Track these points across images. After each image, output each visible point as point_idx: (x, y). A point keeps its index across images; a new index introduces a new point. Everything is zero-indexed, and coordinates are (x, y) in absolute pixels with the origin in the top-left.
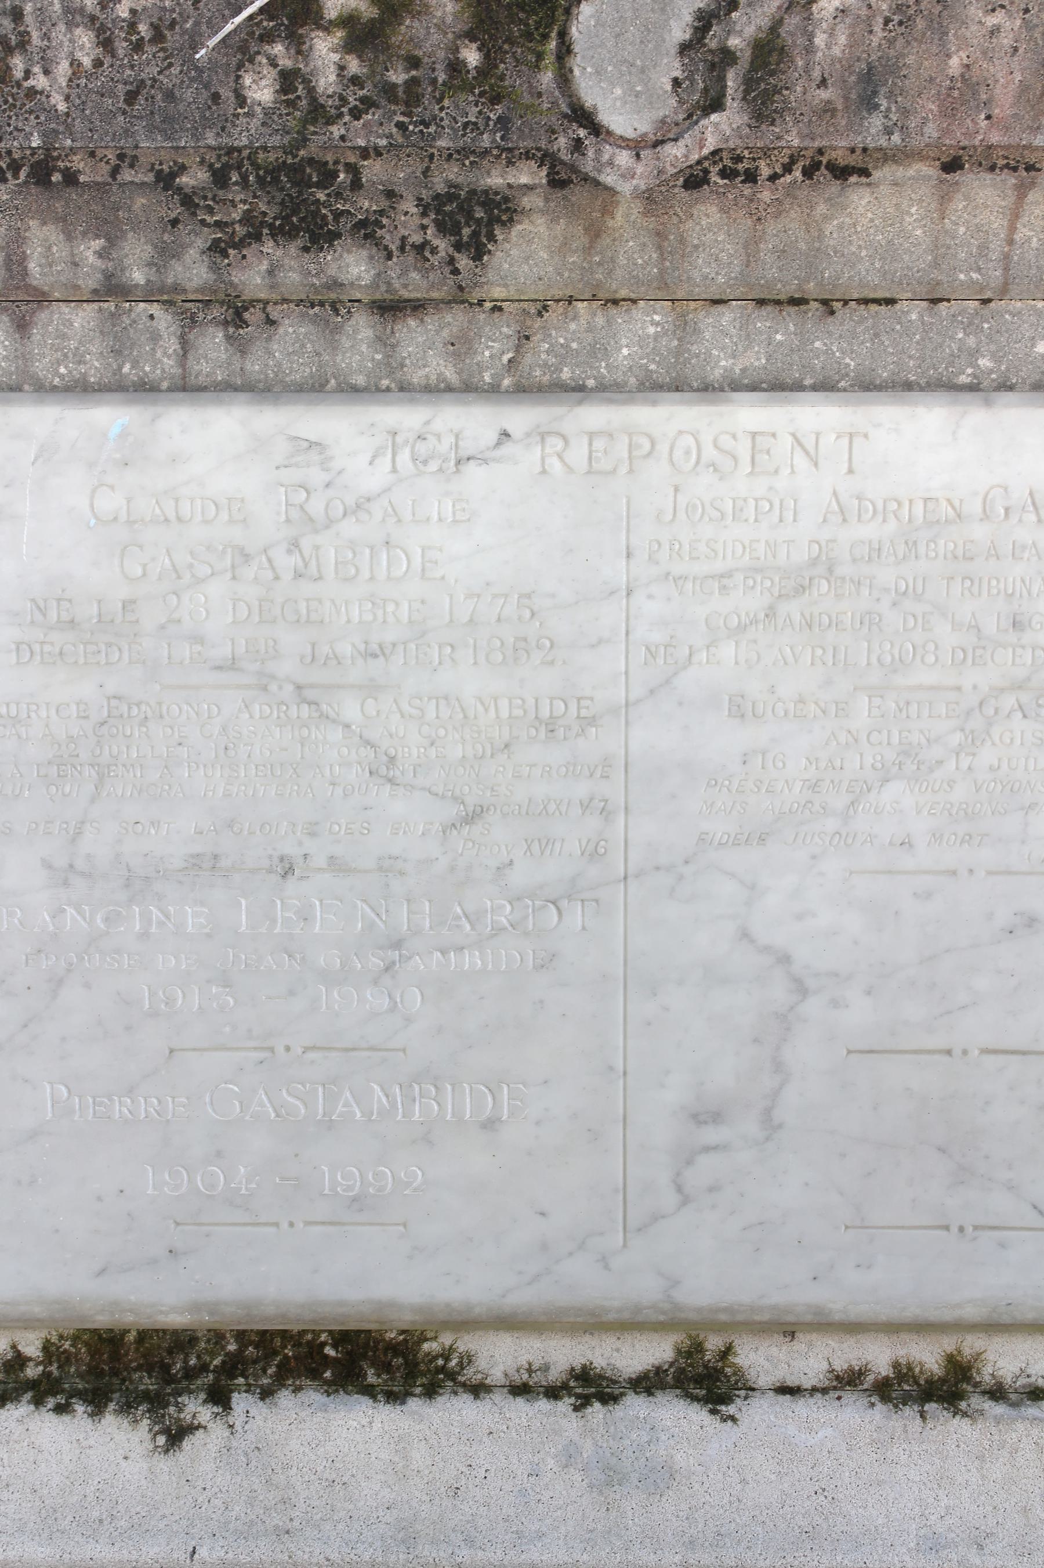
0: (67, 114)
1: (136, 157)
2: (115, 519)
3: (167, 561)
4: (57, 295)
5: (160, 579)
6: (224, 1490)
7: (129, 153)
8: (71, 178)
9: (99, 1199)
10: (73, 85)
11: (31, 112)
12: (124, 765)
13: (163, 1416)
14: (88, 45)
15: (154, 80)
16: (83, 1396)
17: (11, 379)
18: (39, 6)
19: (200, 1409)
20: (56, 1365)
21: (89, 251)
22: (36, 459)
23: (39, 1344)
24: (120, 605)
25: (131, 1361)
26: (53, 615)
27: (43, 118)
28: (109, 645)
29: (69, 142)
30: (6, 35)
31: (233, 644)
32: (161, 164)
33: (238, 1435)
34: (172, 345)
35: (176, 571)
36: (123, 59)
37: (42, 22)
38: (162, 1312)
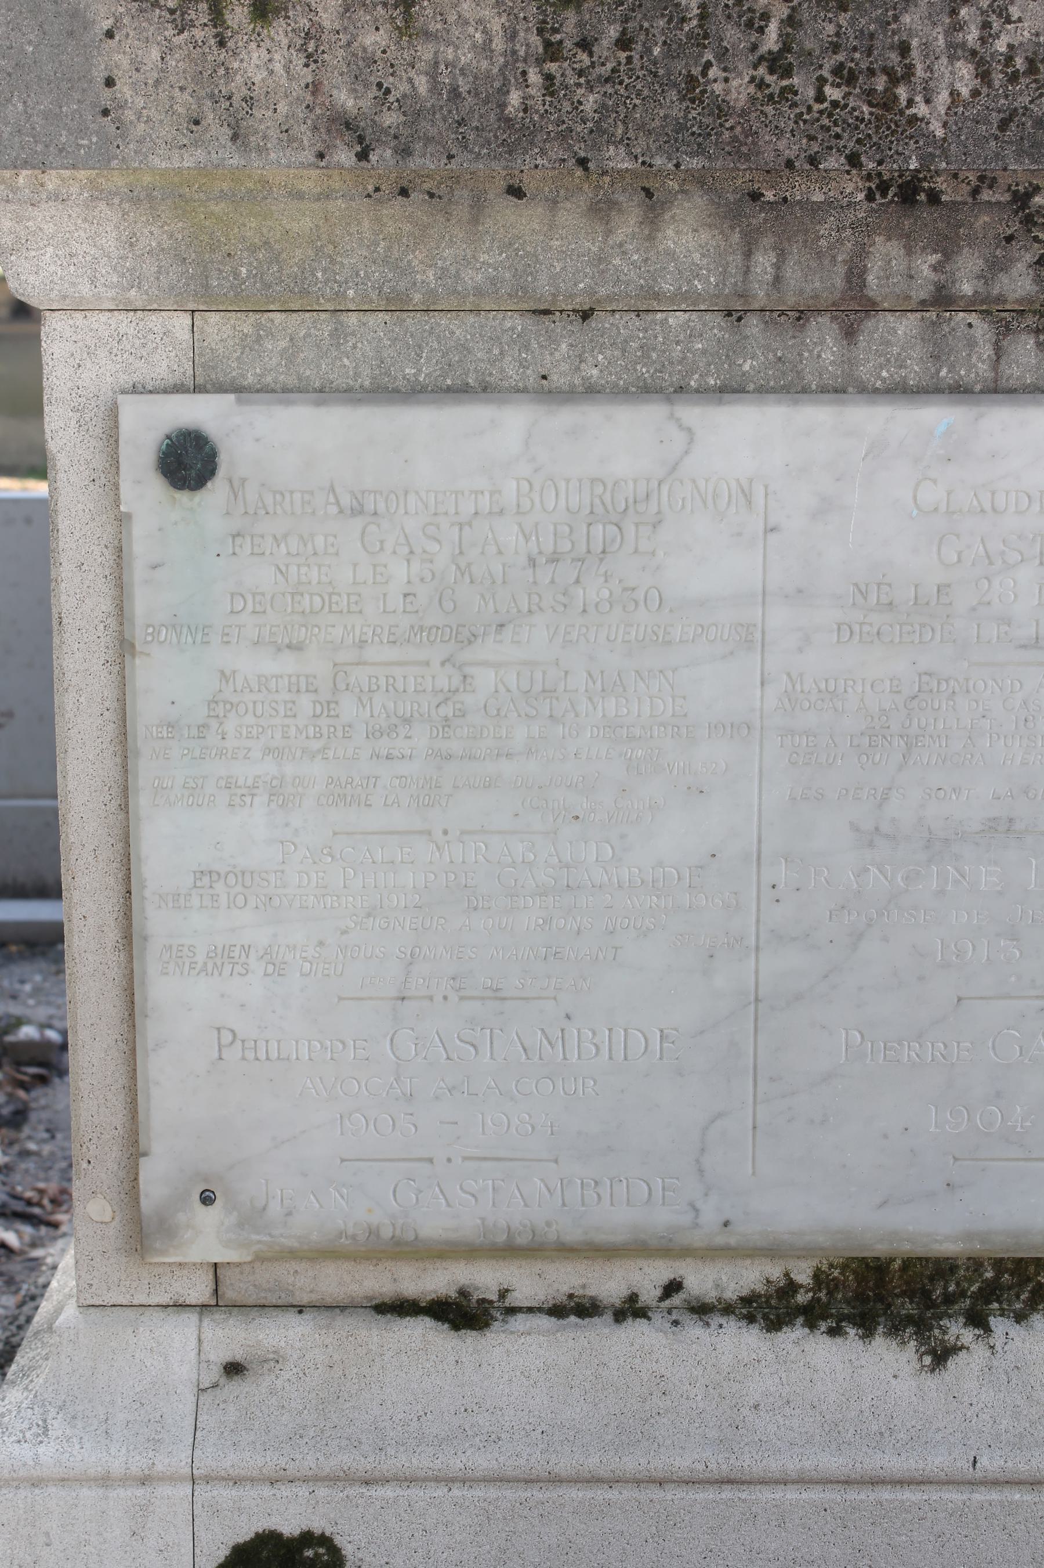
0: (944, 140)
1: (995, 178)
2: (936, 509)
3: (981, 548)
4: (886, 305)
5: (973, 564)
6: (989, 1405)
7: (988, 174)
8: (934, 198)
9: (885, 1136)
10: (952, 113)
11: (911, 137)
12: (931, 736)
13: (929, 1338)
14: (967, 77)
15: (1026, 108)
16: (851, 1319)
17: (837, 381)
18: (924, 41)
19: (962, 1331)
20: (824, 1292)
21: (925, 264)
22: (866, 455)
23: (810, 1272)
24: (935, 589)
25: (895, 1288)
26: (873, 599)
27: (921, 143)
28: (923, 625)
29: (944, 165)
30: (893, 67)
31: (1037, 624)
32: (1017, 185)
33: (998, 1356)
34: (988, 351)
35: (988, 557)
36: (998, 90)
37: (926, 56)
38: (937, 1241)
